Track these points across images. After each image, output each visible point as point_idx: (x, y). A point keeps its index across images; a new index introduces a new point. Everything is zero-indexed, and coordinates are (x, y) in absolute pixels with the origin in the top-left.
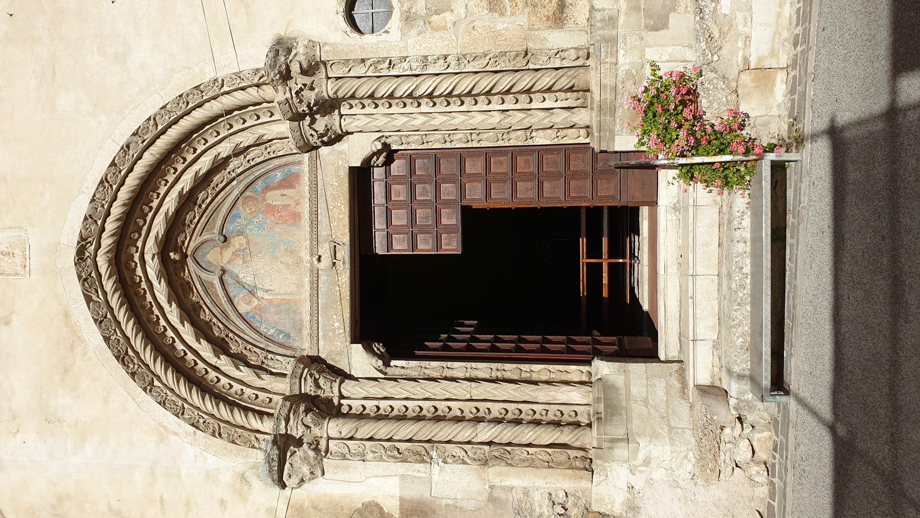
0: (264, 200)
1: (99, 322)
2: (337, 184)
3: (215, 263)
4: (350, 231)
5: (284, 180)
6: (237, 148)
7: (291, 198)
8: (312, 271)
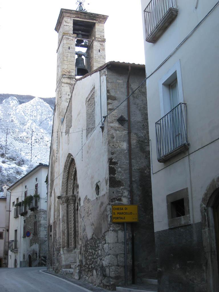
1: (66, 161)
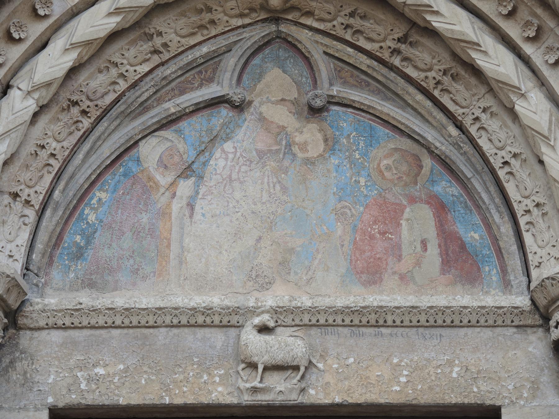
0: (412, 200)
2: (454, 375)
3: (260, 86)
4: (338, 405)
5: (463, 246)
6: (538, 138)
7: (418, 263)
8: (236, 311)
